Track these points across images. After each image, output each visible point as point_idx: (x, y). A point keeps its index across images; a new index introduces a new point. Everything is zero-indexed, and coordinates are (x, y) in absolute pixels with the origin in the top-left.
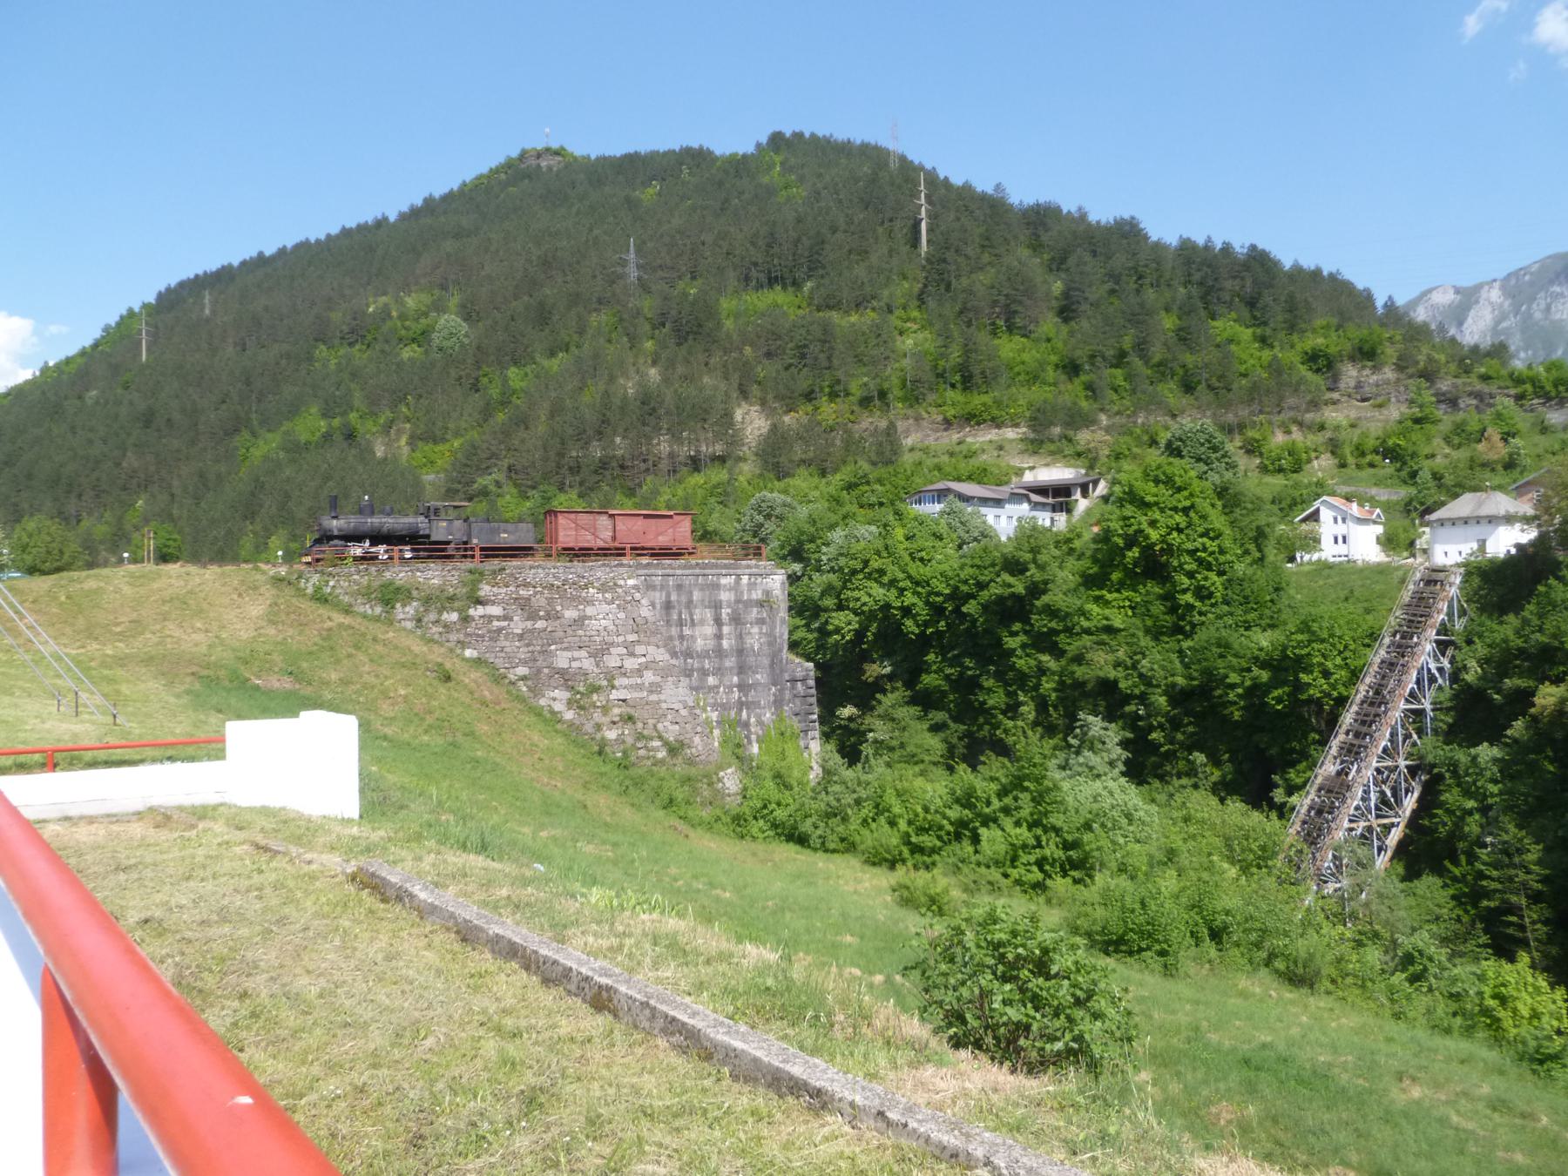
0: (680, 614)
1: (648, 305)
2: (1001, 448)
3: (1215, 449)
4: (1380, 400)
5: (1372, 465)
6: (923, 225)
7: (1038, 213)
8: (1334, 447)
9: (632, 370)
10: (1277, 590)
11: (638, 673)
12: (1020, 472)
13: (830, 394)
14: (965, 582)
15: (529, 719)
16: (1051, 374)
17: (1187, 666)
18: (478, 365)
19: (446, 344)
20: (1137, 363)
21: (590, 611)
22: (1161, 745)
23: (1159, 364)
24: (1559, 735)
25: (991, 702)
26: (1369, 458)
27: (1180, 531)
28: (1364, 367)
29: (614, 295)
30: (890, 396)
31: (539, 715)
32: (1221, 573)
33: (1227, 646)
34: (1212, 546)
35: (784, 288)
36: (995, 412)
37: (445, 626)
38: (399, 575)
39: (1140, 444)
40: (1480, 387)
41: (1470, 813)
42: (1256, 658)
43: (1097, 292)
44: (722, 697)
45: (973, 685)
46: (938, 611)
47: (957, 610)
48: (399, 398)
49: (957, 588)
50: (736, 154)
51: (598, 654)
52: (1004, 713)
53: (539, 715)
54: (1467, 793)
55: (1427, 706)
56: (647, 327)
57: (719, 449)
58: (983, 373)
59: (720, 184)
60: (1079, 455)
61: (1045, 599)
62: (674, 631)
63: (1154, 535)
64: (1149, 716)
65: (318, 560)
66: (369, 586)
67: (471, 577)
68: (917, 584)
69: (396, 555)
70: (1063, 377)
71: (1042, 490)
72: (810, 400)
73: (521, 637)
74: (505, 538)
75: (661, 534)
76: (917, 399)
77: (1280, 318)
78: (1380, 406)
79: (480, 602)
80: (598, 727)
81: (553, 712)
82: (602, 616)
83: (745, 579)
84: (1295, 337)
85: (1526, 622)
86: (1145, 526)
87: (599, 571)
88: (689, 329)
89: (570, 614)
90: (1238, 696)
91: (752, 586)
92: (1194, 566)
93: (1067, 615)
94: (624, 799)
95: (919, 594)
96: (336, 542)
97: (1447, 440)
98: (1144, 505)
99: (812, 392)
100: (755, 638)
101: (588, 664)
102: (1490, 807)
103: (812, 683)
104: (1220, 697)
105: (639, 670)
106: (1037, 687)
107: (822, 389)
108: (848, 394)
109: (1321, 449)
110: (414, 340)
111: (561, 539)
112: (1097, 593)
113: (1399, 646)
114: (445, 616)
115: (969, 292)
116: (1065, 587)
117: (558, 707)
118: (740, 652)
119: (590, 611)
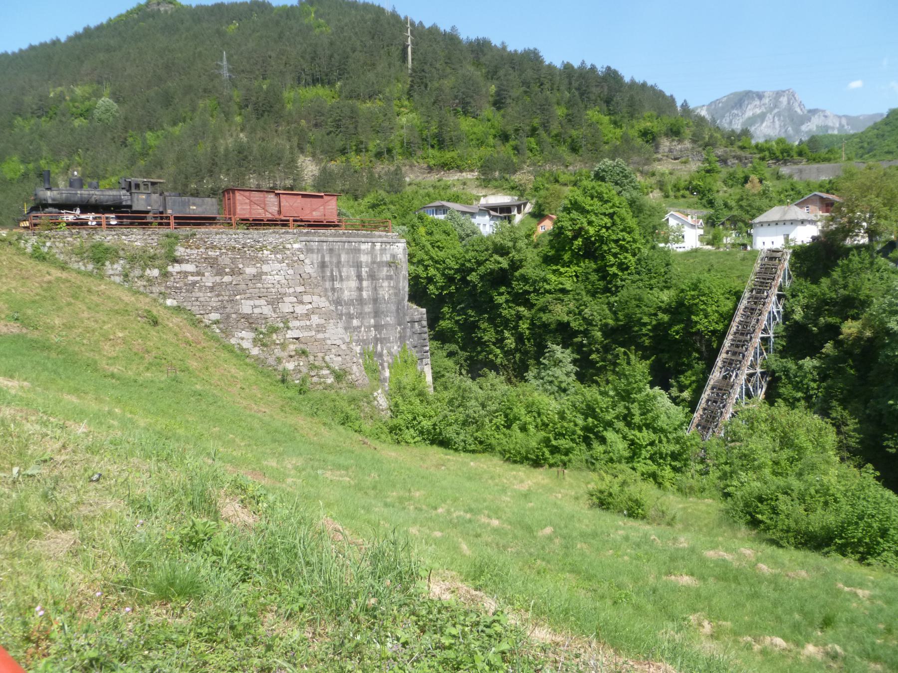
0: (332, 271)
1: (237, 95)
2: (465, 184)
3: (626, 177)
4: (683, 159)
5: (683, 196)
6: (409, 49)
7: (479, 43)
8: (661, 186)
9: (228, 134)
10: (667, 265)
11: (307, 316)
12: (478, 199)
13: (356, 151)
14: (469, 261)
15: (225, 355)
16: (491, 141)
17: (615, 313)
18: (126, 129)
19: (104, 116)
20: (544, 135)
21: (265, 268)
22: (597, 362)
23: (556, 135)
24: (857, 351)
25: (486, 338)
26: (682, 192)
27: (607, 228)
28: (673, 140)
29: (214, 87)
30: (394, 151)
31: (232, 352)
32: (634, 255)
33: (640, 299)
34: (628, 237)
35: (323, 86)
36: (459, 163)
37: (148, 280)
38: (108, 238)
39: (549, 182)
40: (739, 153)
41: (798, 400)
42: (660, 308)
43: (516, 92)
44: (363, 335)
45: (474, 326)
46: (450, 280)
47: (463, 280)
48: (72, 151)
49: (463, 265)
50: (286, 6)
51: (275, 301)
52: (494, 344)
53: (232, 352)
54: (797, 388)
55: (772, 335)
56: (236, 108)
57: (289, 183)
58: (451, 139)
59: (277, 23)
60: (513, 188)
61: (521, 271)
62: (328, 285)
63: (592, 231)
64: (590, 344)
65: (35, 225)
66: (81, 247)
67: (168, 240)
68: (436, 262)
69: (104, 222)
70: (499, 142)
71: (494, 209)
72: (344, 154)
73: (212, 289)
74: (194, 209)
75: (314, 210)
76: (411, 154)
77: (625, 110)
78: (685, 163)
79: (176, 261)
80: (279, 360)
81: (242, 349)
82: (275, 272)
83: (378, 246)
84: (634, 122)
85: (835, 282)
86: (585, 225)
87: (271, 237)
88: (265, 109)
89: (250, 271)
90: (649, 330)
91: (383, 251)
92: (617, 250)
93: (535, 281)
94: (316, 419)
95: (438, 269)
96: (50, 209)
97: (725, 182)
98: (583, 211)
99: (345, 149)
100: (385, 291)
101: (267, 310)
102: (811, 397)
103: (425, 323)
104: (637, 331)
105: (307, 315)
106: (516, 327)
107: (351, 148)
108: (367, 151)
109: (654, 186)
110: (81, 115)
111: (238, 211)
112: (554, 268)
113: (756, 298)
114: (148, 272)
115: (440, 89)
116: (533, 264)
117: (246, 344)
118: (375, 300)
119: (265, 268)
